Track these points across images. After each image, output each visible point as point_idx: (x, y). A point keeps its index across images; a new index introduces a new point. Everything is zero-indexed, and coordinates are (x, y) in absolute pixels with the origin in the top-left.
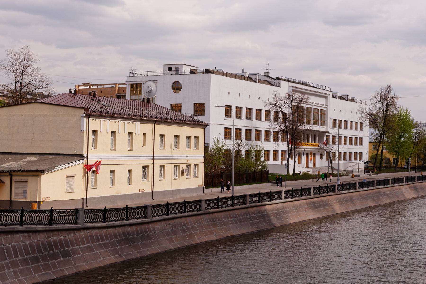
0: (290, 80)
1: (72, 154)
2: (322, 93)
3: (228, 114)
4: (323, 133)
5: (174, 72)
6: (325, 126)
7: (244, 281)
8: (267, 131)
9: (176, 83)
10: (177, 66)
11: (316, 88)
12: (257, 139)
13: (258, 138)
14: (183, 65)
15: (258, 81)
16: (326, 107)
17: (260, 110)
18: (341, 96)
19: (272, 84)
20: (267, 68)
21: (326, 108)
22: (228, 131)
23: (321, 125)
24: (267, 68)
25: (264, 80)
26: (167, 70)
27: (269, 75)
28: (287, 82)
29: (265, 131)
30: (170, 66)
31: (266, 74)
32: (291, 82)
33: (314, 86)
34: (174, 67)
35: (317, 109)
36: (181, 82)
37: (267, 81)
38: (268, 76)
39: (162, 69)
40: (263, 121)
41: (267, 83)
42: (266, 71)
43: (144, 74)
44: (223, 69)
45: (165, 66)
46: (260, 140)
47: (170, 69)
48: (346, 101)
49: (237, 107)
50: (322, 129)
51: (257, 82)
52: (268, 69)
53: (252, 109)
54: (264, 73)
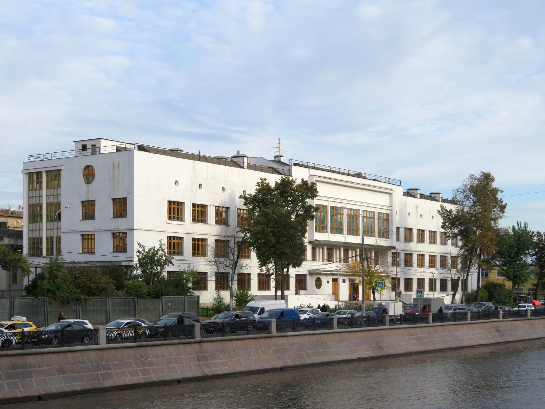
0: (311, 165)
1: (104, 261)
2: (335, 179)
3: (200, 218)
4: (385, 249)
5: (88, 151)
6: (388, 238)
7: (505, 408)
8: (431, 255)
9: (87, 167)
10: (93, 143)
11: (378, 181)
12: (431, 266)
13: (432, 265)
14: (101, 140)
15: (440, 199)
16: (390, 209)
17: (435, 232)
18: (429, 195)
19: (280, 172)
20: (278, 150)
21: (390, 210)
22: (178, 243)
23: (332, 232)
24: (278, 150)
25: (268, 167)
26: (81, 148)
27: (282, 160)
28: (307, 169)
29: (430, 255)
30: (84, 143)
31: (277, 159)
32: (314, 168)
33: (376, 178)
34: (89, 145)
35: (372, 212)
36: (94, 167)
37: (272, 168)
38: (280, 162)
39: (73, 147)
40: (401, 241)
41: (274, 170)
42: (278, 154)
43: (48, 157)
44: (181, 148)
45: (76, 142)
46: (435, 266)
47: (84, 148)
48: (437, 202)
49: (194, 205)
50: (383, 242)
51: (440, 201)
52: (279, 151)
53: (413, 229)
54: (275, 157)
